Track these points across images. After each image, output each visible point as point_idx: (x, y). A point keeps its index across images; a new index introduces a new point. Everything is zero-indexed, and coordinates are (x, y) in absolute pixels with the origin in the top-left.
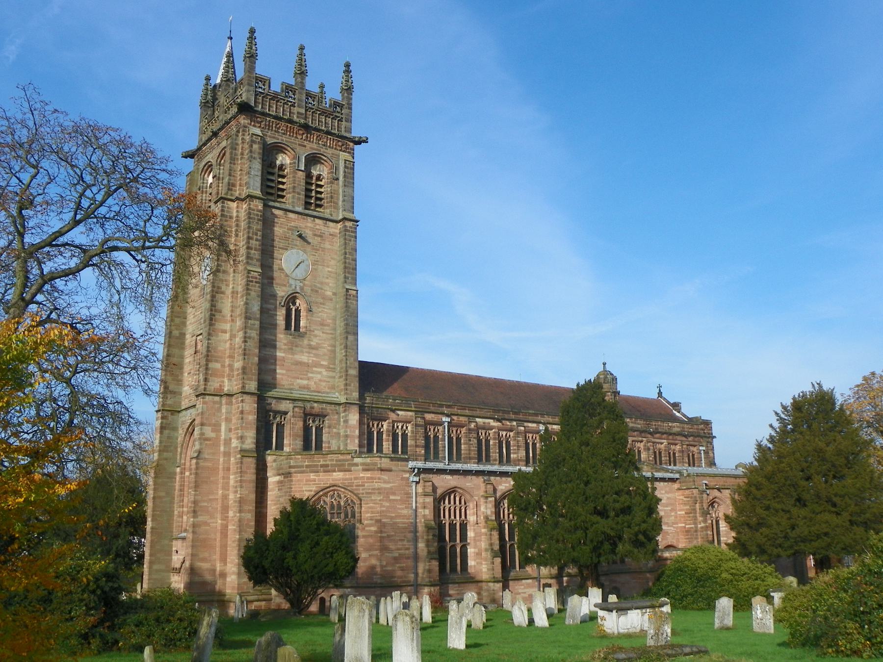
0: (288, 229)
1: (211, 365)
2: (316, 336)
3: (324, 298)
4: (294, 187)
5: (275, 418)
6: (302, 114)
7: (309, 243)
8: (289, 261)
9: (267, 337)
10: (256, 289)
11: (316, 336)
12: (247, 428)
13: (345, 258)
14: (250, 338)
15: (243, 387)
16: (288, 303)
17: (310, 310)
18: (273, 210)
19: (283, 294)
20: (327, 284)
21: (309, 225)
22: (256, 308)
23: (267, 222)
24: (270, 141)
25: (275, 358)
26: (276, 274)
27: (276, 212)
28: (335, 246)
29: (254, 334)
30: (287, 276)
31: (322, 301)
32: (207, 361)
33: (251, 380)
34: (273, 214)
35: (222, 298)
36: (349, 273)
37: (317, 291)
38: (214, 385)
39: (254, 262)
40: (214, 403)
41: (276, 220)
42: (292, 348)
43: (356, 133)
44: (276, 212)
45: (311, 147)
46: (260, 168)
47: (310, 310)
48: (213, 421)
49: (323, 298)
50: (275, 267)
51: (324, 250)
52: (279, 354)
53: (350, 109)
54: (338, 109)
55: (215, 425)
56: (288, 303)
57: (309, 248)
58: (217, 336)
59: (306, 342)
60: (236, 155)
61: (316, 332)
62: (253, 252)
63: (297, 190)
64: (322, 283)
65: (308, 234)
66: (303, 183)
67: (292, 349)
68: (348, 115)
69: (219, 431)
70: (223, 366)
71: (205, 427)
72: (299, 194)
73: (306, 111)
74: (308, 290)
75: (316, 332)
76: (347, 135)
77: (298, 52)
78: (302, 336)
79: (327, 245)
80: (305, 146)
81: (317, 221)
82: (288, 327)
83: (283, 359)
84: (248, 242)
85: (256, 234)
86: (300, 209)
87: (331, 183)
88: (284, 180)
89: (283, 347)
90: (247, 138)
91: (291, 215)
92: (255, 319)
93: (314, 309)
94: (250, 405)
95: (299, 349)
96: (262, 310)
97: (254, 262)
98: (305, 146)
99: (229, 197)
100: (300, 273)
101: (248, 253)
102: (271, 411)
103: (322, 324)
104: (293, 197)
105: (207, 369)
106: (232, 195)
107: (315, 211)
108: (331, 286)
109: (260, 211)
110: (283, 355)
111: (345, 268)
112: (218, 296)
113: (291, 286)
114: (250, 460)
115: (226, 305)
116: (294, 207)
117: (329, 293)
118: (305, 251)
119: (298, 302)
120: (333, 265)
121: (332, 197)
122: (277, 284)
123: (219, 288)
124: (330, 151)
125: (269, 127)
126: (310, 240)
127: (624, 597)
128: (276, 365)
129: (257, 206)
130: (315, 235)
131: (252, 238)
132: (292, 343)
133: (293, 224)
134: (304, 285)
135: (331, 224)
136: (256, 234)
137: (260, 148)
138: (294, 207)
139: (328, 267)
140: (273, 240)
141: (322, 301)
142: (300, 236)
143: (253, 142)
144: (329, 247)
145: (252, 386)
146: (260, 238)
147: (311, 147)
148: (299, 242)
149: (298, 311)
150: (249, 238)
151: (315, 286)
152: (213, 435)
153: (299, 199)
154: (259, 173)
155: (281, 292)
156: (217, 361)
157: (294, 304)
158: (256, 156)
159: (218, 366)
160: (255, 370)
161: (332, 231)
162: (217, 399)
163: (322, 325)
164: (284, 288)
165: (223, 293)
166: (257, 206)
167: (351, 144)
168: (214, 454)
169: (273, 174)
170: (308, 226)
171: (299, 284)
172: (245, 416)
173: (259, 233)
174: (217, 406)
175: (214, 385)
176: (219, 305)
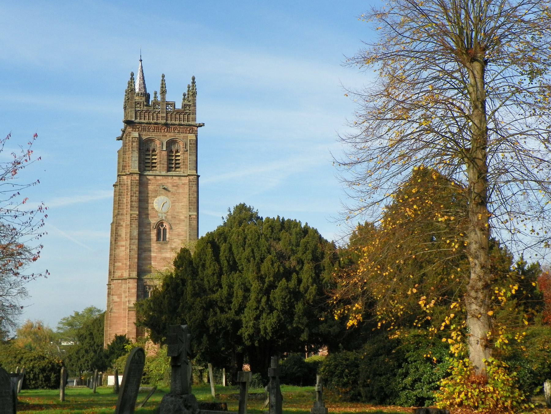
0: (157, 186)
1: (116, 264)
2: (174, 242)
3: (180, 220)
4: (160, 161)
5: (150, 289)
6: (164, 117)
7: (169, 191)
8: (159, 204)
9: (146, 246)
10: (136, 223)
11: (174, 242)
12: (131, 296)
13: (189, 197)
14: (132, 249)
15: (129, 275)
16: (159, 226)
17: (171, 228)
18: (148, 177)
19: (155, 222)
20: (181, 212)
21: (170, 181)
22: (135, 233)
23: (142, 184)
24: (144, 138)
25: (150, 257)
26: (150, 212)
27: (149, 177)
28: (184, 193)
29: (135, 247)
30: (157, 211)
31: (178, 222)
32: (114, 262)
33: (133, 271)
34: (148, 179)
35: (121, 229)
36: (191, 205)
37: (175, 217)
38: (118, 274)
39: (135, 208)
40: (119, 283)
41: (149, 182)
42: (160, 250)
43: (198, 122)
44: (149, 177)
45: (170, 136)
46: (138, 156)
47: (171, 228)
48: (118, 293)
49: (179, 221)
50: (150, 208)
51: (179, 193)
52: (153, 254)
53: (195, 106)
54: (188, 108)
55: (119, 295)
56: (159, 226)
57: (170, 194)
58: (119, 249)
59: (169, 246)
60: (126, 149)
61: (175, 240)
62: (134, 203)
63: (162, 162)
64: (178, 212)
65: (169, 186)
66: (166, 157)
67: (160, 251)
68: (194, 110)
69: (122, 297)
70: (123, 264)
71: (114, 296)
72: (163, 164)
73: (167, 114)
74: (169, 217)
75: (175, 240)
76: (193, 123)
77: (162, 78)
78: (167, 243)
79: (181, 191)
80: (166, 136)
81: (174, 178)
82: (158, 239)
83: (156, 257)
84: (131, 199)
85: (136, 193)
86: (164, 173)
87: (184, 154)
88: (156, 157)
89: (156, 250)
90: (131, 139)
91: (158, 178)
92: (135, 239)
93: (173, 227)
94: (133, 285)
95: (165, 250)
96: (140, 233)
97: (135, 208)
98: (166, 136)
99: (123, 174)
100: (165, 210)
101: (131, 204)
102: (147, 285)
103: (179, 235)
104: (160, 167)
105: (114, 266)
106: (125, 172)
107: (175, 171)
108: (183, 212)
109: (137, 180)
110: (155, 255)
111: (189, 203)
112: (119, 228)
113: (159, 217)
114: (133, 312)
115: (124, 232)
116: (160, 172)
117: (182, 218)
118: (167, 196)
119: (164, 224)
120: (184, 201)
121: (184, 162)
122: (151, 217)
123: (119, 223)
124: (182, 135)
125: (144, 129)
126: (170, 190)
127: (196, 355)
128: (151, 260)
129: (135, 178)
130: (173, 186)
131: (133, 196)
132: (161, 248)
133: (160, 182)
134: (167, 215)
135: (183, 178)
136: (136, 193)
137: (137, 144)
138: (160, 172)
139: (182, 202)
140: (148, 193)
141: (178, 222)
142: (164, 189)
143: (133, 142)
144: (182, 191)
145: (134, 274)
146: (137, 195)
147: (170, 136)
148: (163, 192)
149: (165, 230)
150: (131, 196)
151: (174, 215)
152: (118, 300)
153: (163, 167)
154: (137, 159)
155: (153, 221)
156: (119, 262)
157: (162, 226)
158: (135, 149)
159: (120, 264)
160: (135, 266)
161: (183, 182)
162: (120, 281)
163: (178, 235)
164: (155, 219)
165: (122, 226)
166: (135, 178)
167: (196, 128)
168: (118, 309)
169: (149, 155)
170: (168, 182)
171: (164, 215)
172: (130, 290)
173: (137, 193)
174: (120, 285)
175: (118, 274)
176: (119, 233)
